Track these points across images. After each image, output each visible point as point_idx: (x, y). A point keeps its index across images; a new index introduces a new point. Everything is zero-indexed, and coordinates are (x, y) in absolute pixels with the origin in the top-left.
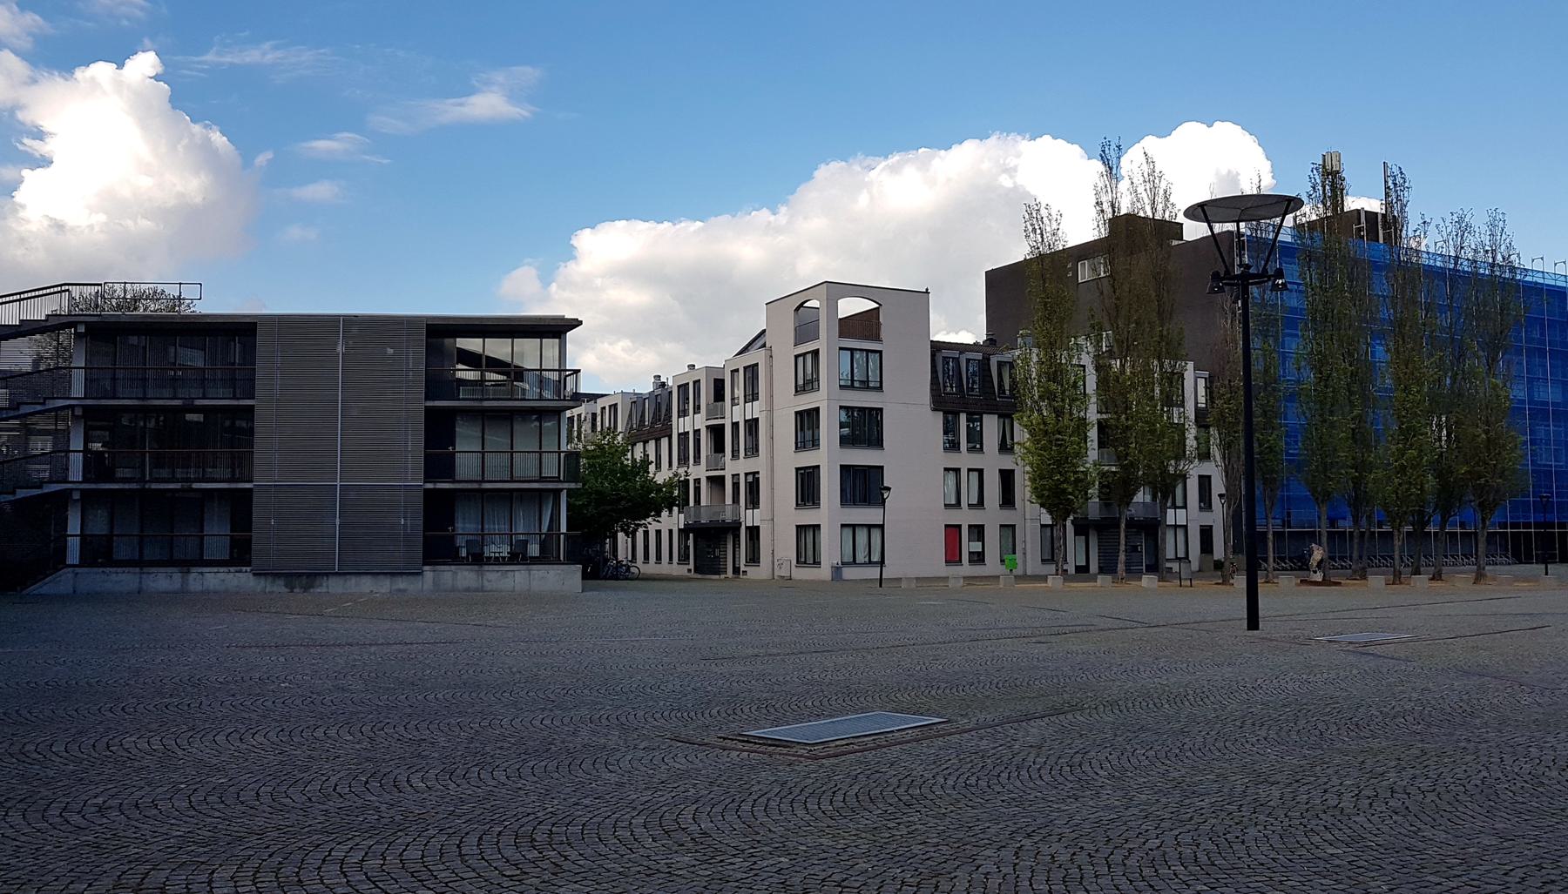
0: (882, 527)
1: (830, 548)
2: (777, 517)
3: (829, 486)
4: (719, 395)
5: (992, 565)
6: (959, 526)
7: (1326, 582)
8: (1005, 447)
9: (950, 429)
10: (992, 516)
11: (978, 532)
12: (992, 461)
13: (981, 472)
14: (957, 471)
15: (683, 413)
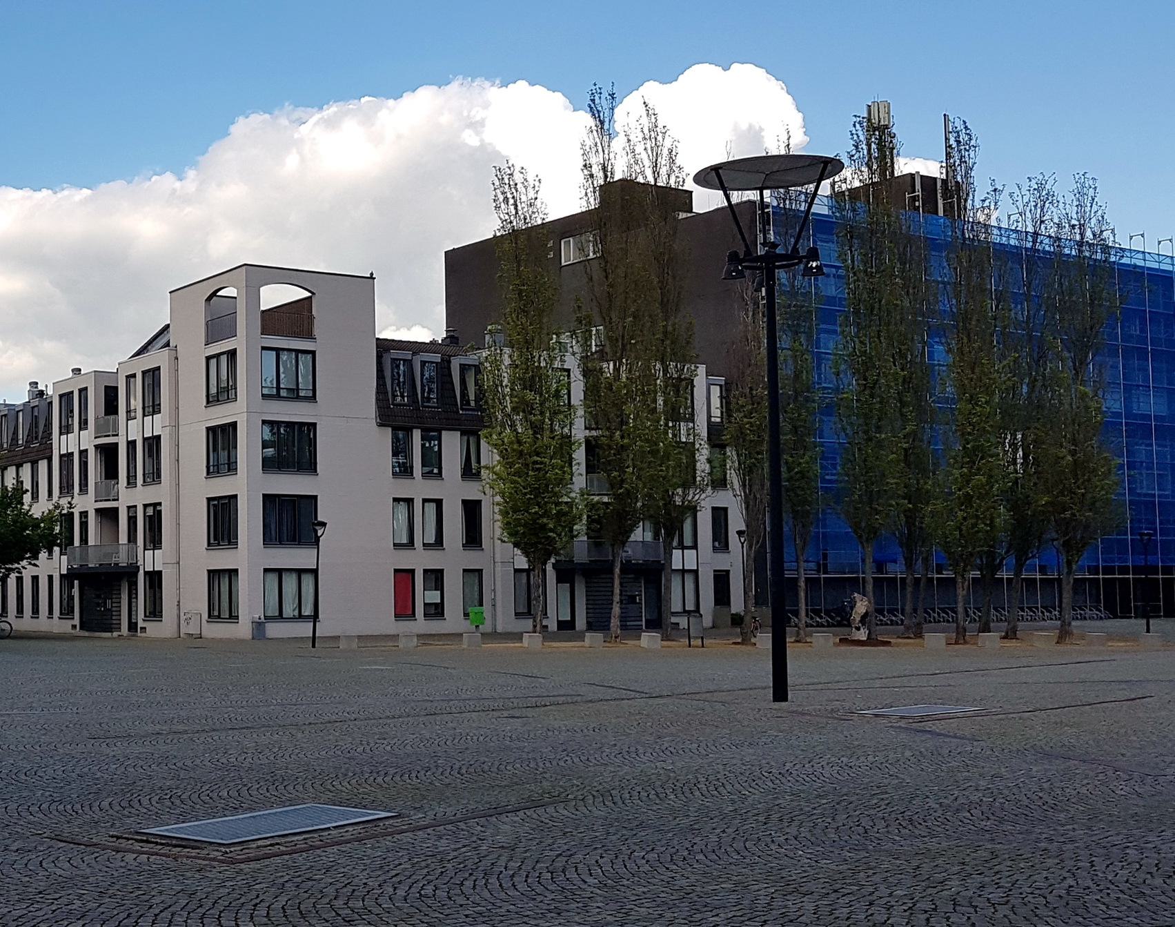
0: (315, 572)
1: (251, 598)
2: (184, 559)
3: (249, 520)
4: (111, 406)
5: (453, 620)
6: (412, 572)
7: (871, 642)
8: (470, 472)
9: (400, 449)
10: (454, 559)
11: (435, 578)
12: (453, 489)
13: (439, 503)
14: (409, 502)
15: (66, 429)
